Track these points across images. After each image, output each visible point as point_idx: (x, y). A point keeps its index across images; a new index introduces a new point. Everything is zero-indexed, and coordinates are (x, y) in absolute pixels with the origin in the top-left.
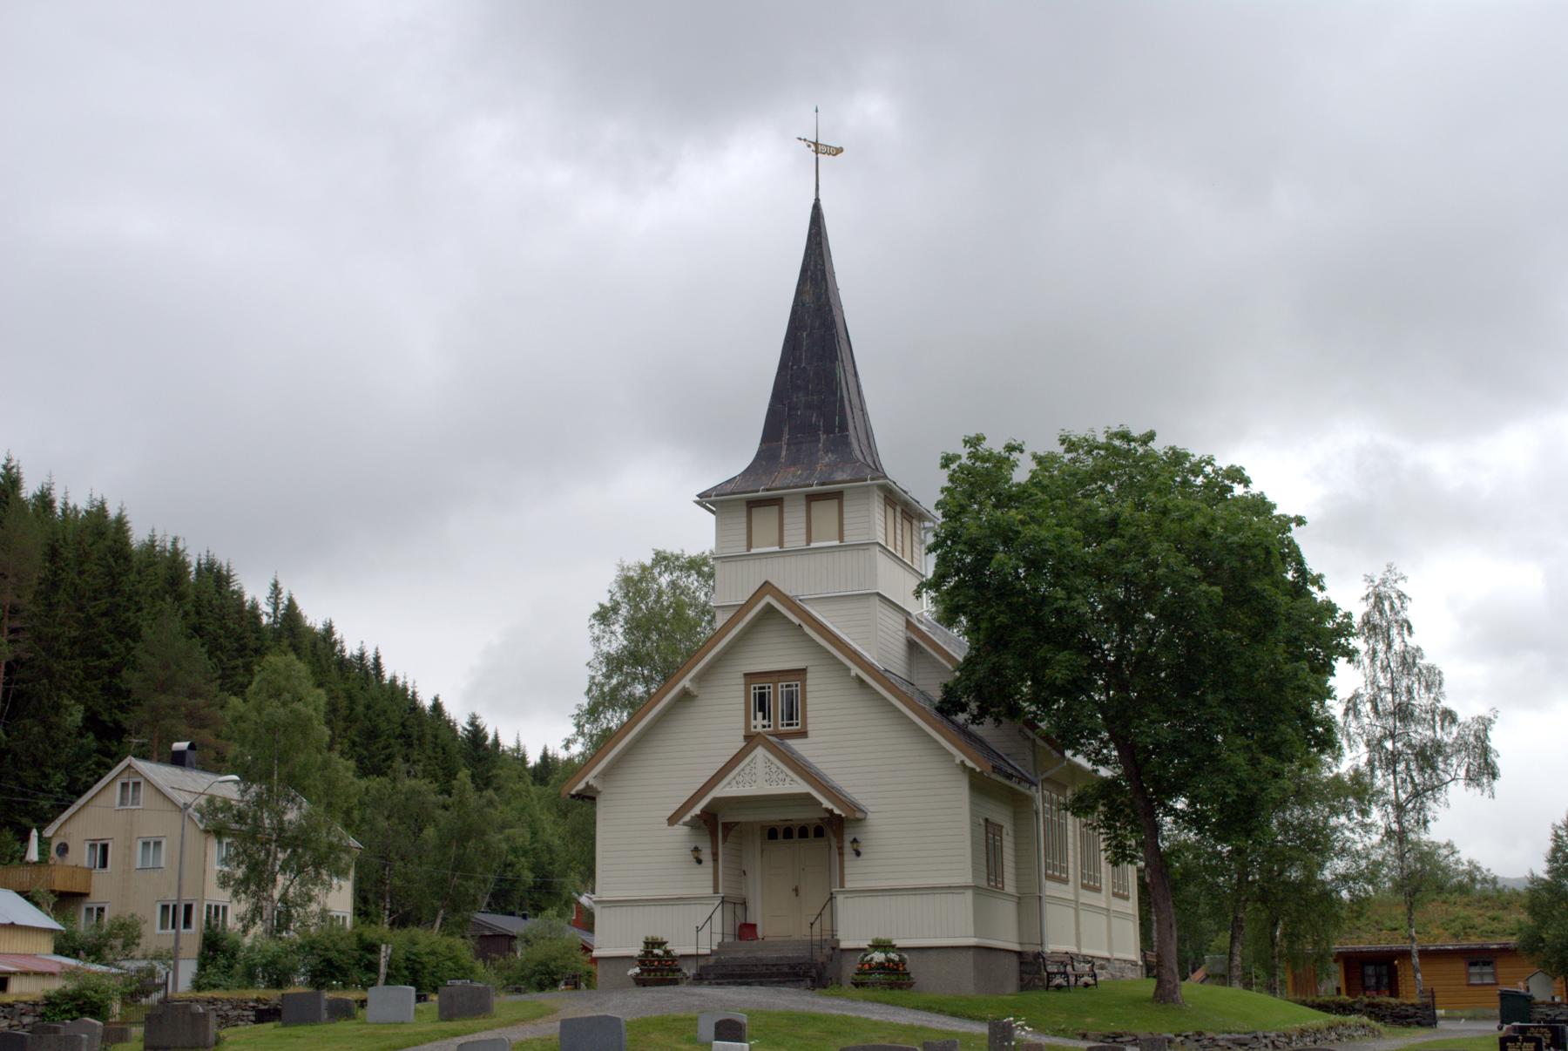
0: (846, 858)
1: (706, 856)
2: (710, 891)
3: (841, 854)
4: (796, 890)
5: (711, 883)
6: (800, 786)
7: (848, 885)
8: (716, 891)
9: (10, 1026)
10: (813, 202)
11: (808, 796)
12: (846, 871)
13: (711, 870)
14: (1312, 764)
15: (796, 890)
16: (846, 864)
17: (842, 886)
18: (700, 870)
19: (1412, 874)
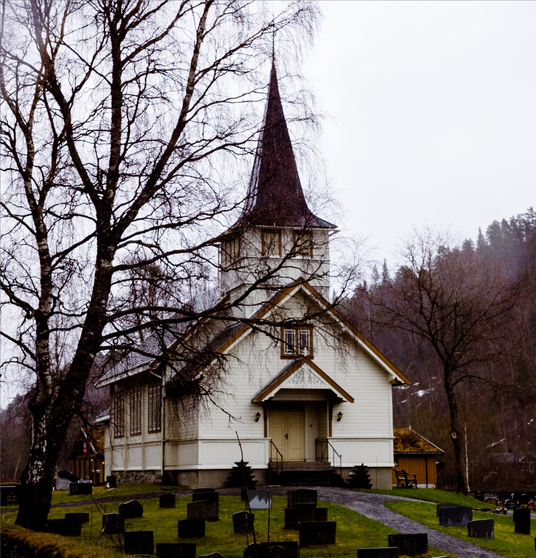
0: (333, 421)
1: (261, 419)
2: (262, 436)
3: (331, 420)
4: (287, 436)
5: (263, 432)
6: (327, 386)
7: (334, 435)
8: (266, 436)
9: (429, 448)
10: (478, 234)
11: (330, 390)
12: (333, 428)
13: (263, 425)
14: (473, 252)
15: (287, 436)
16: (333, 425)
17: (330, 435)
18: (257, 424)
19: (59, 476)
